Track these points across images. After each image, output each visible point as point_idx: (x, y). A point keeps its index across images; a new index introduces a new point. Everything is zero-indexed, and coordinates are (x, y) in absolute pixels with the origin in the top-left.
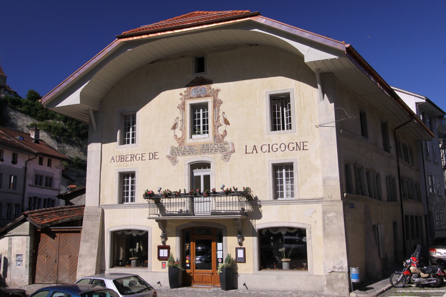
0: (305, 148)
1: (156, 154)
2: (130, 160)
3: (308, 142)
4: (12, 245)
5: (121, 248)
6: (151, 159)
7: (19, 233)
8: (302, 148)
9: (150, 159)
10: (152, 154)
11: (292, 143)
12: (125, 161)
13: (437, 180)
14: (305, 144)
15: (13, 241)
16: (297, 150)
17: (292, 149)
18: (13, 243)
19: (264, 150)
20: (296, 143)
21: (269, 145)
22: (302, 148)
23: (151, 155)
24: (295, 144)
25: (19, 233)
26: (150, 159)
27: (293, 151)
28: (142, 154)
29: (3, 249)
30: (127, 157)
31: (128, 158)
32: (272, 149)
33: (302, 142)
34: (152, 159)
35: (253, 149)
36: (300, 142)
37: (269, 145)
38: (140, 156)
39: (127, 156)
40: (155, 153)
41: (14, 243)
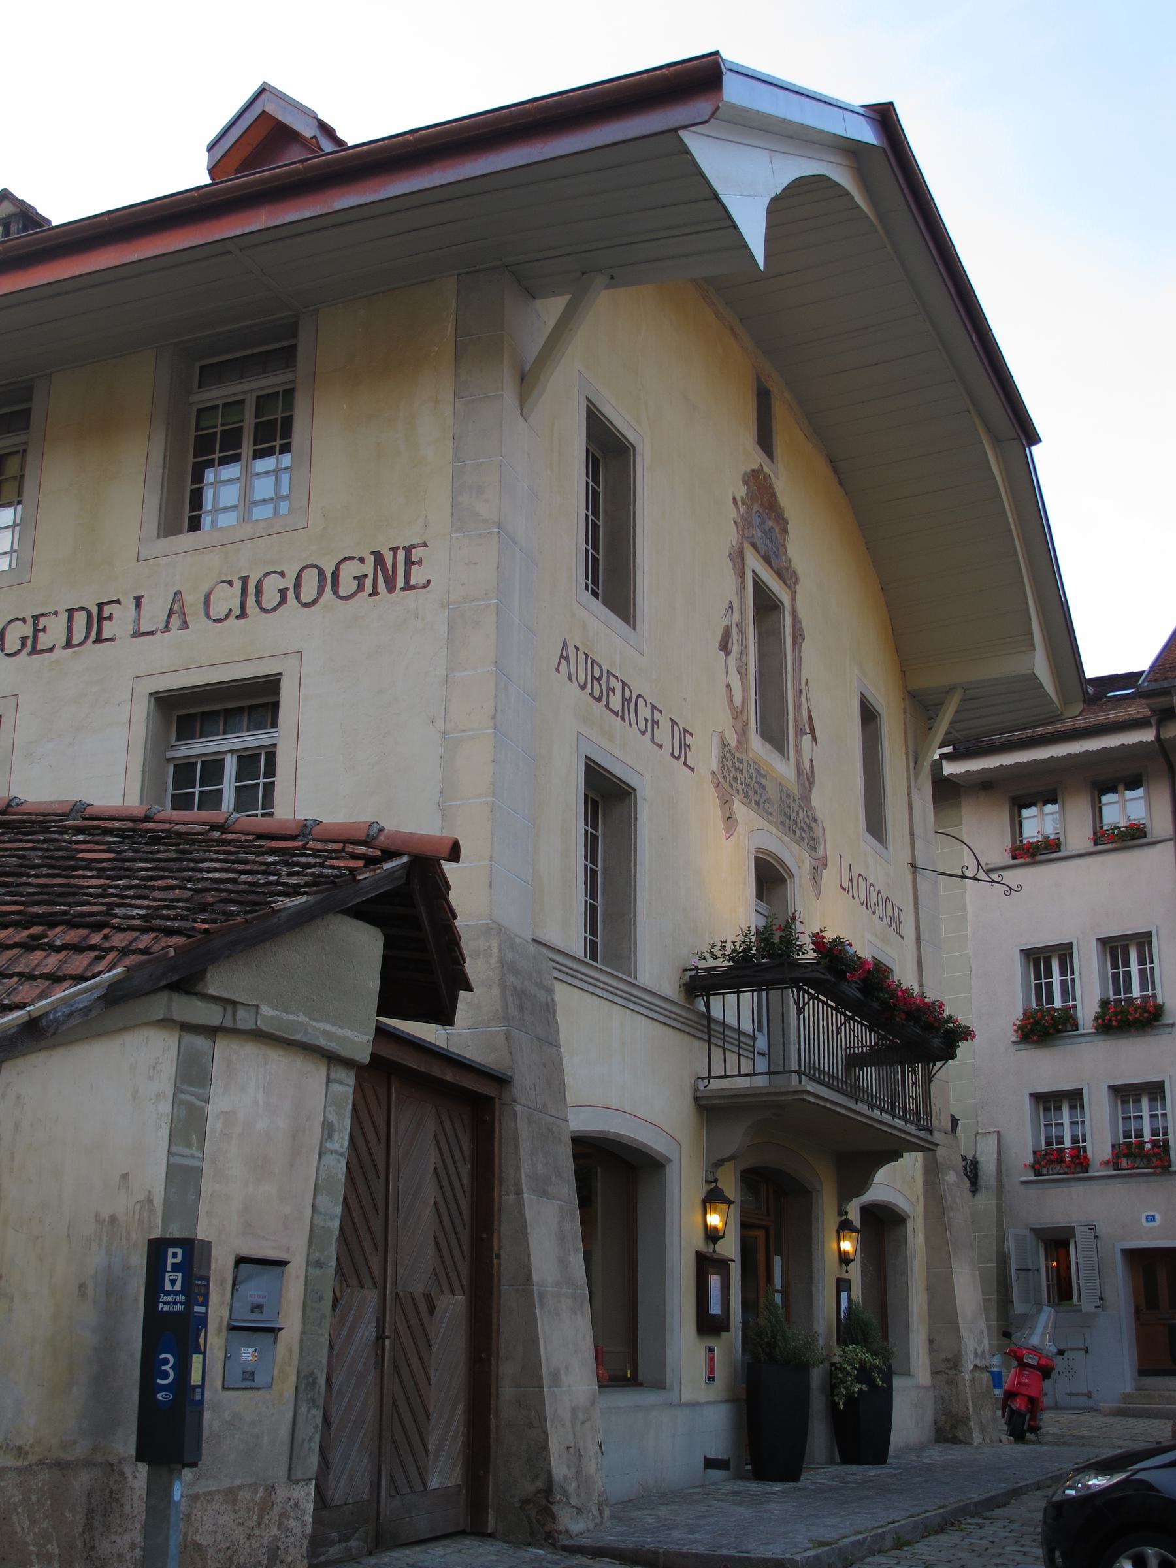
0: (417, 577)
1: (106, 614)
2: (237, 612)
3: (121, 600)
4: (202, 1147)
5: (599, 1170)
6: (75, 641)
7: (302, 1018)
8: (400, 582)
9: (69, 645)
10: (84, 613)
11: (17, 619)
12: (403, 589)
13: (159, 856)
14: (416, 554)
15: (220, 1101)
16: (375, 593)
17: (355, 585)
18: (214, 1125)
19: (218, 610)
20: (372, 553)
21: (245, 580)
22: (400, 582)
23: (80, 619)
24: (370, 560)
25: (302, 1018)
26: (69, 645)
27: (356, 598)
28: (36, 618)
29: (125, 1177)
30: (41, 627)
31: (110, 618)
32: (258, 602)
33: (404, 548)
34: (80, 644)
35: (171, 612)
36: (394, 550)
37: (245, 580)
38: (27, 630)
39: (106, 608)
40: (100, 606)
41: (228, 1116)
